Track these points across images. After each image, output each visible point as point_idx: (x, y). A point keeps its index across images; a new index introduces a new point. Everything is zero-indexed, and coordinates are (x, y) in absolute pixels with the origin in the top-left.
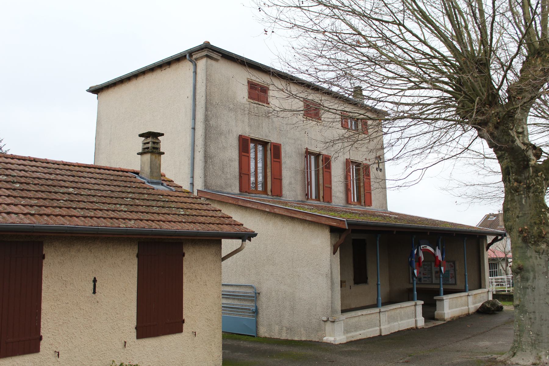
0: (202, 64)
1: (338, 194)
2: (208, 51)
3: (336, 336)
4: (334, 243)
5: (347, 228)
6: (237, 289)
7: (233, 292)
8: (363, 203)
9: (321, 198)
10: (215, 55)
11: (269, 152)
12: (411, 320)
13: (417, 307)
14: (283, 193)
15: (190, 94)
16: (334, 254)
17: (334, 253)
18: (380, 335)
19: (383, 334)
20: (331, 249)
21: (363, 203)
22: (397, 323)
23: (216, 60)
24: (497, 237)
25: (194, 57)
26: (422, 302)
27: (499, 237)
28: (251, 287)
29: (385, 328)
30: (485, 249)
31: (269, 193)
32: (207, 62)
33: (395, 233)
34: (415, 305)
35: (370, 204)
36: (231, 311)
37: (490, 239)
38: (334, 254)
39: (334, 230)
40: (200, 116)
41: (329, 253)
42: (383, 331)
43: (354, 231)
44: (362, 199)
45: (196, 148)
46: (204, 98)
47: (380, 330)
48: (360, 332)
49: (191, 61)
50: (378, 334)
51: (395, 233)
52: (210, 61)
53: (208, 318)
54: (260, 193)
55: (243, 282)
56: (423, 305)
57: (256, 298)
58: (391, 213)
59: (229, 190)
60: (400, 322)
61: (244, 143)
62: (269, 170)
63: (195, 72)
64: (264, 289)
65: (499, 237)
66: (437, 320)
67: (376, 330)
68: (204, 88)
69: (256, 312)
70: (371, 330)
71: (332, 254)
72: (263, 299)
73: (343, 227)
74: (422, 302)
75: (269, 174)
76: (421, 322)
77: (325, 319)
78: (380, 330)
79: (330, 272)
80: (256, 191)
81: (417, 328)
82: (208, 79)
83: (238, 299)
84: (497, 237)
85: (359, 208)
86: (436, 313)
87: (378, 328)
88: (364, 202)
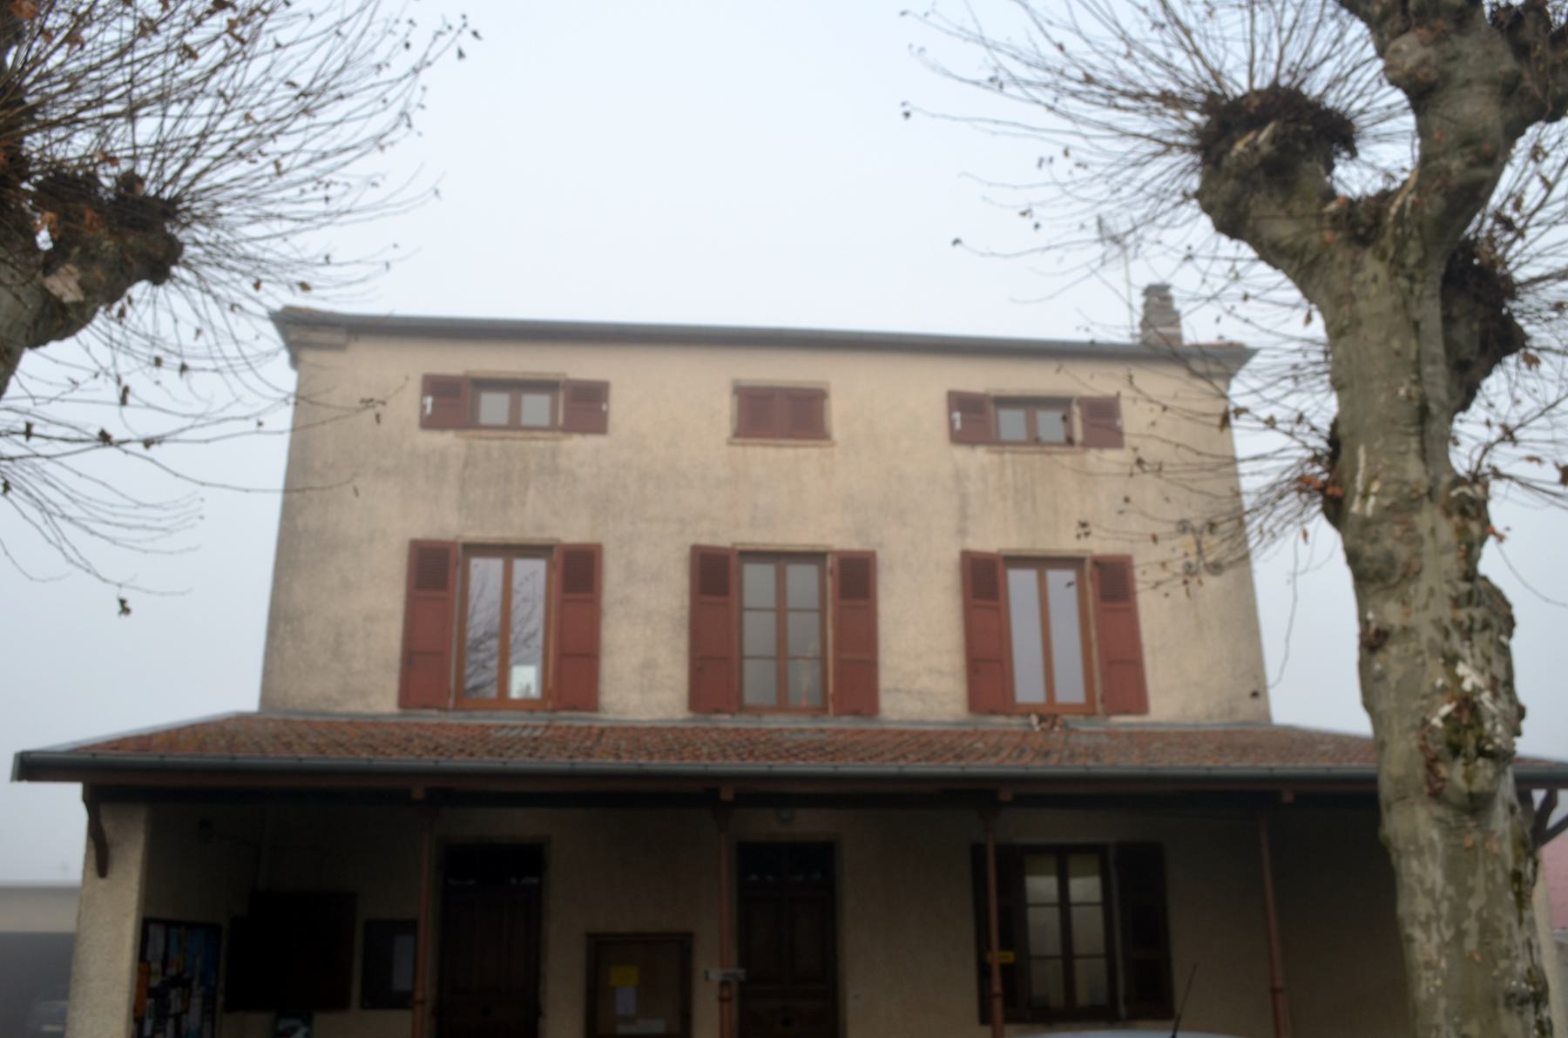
23: (340, 347)
35: (1139, 703)
59: (355, 706)
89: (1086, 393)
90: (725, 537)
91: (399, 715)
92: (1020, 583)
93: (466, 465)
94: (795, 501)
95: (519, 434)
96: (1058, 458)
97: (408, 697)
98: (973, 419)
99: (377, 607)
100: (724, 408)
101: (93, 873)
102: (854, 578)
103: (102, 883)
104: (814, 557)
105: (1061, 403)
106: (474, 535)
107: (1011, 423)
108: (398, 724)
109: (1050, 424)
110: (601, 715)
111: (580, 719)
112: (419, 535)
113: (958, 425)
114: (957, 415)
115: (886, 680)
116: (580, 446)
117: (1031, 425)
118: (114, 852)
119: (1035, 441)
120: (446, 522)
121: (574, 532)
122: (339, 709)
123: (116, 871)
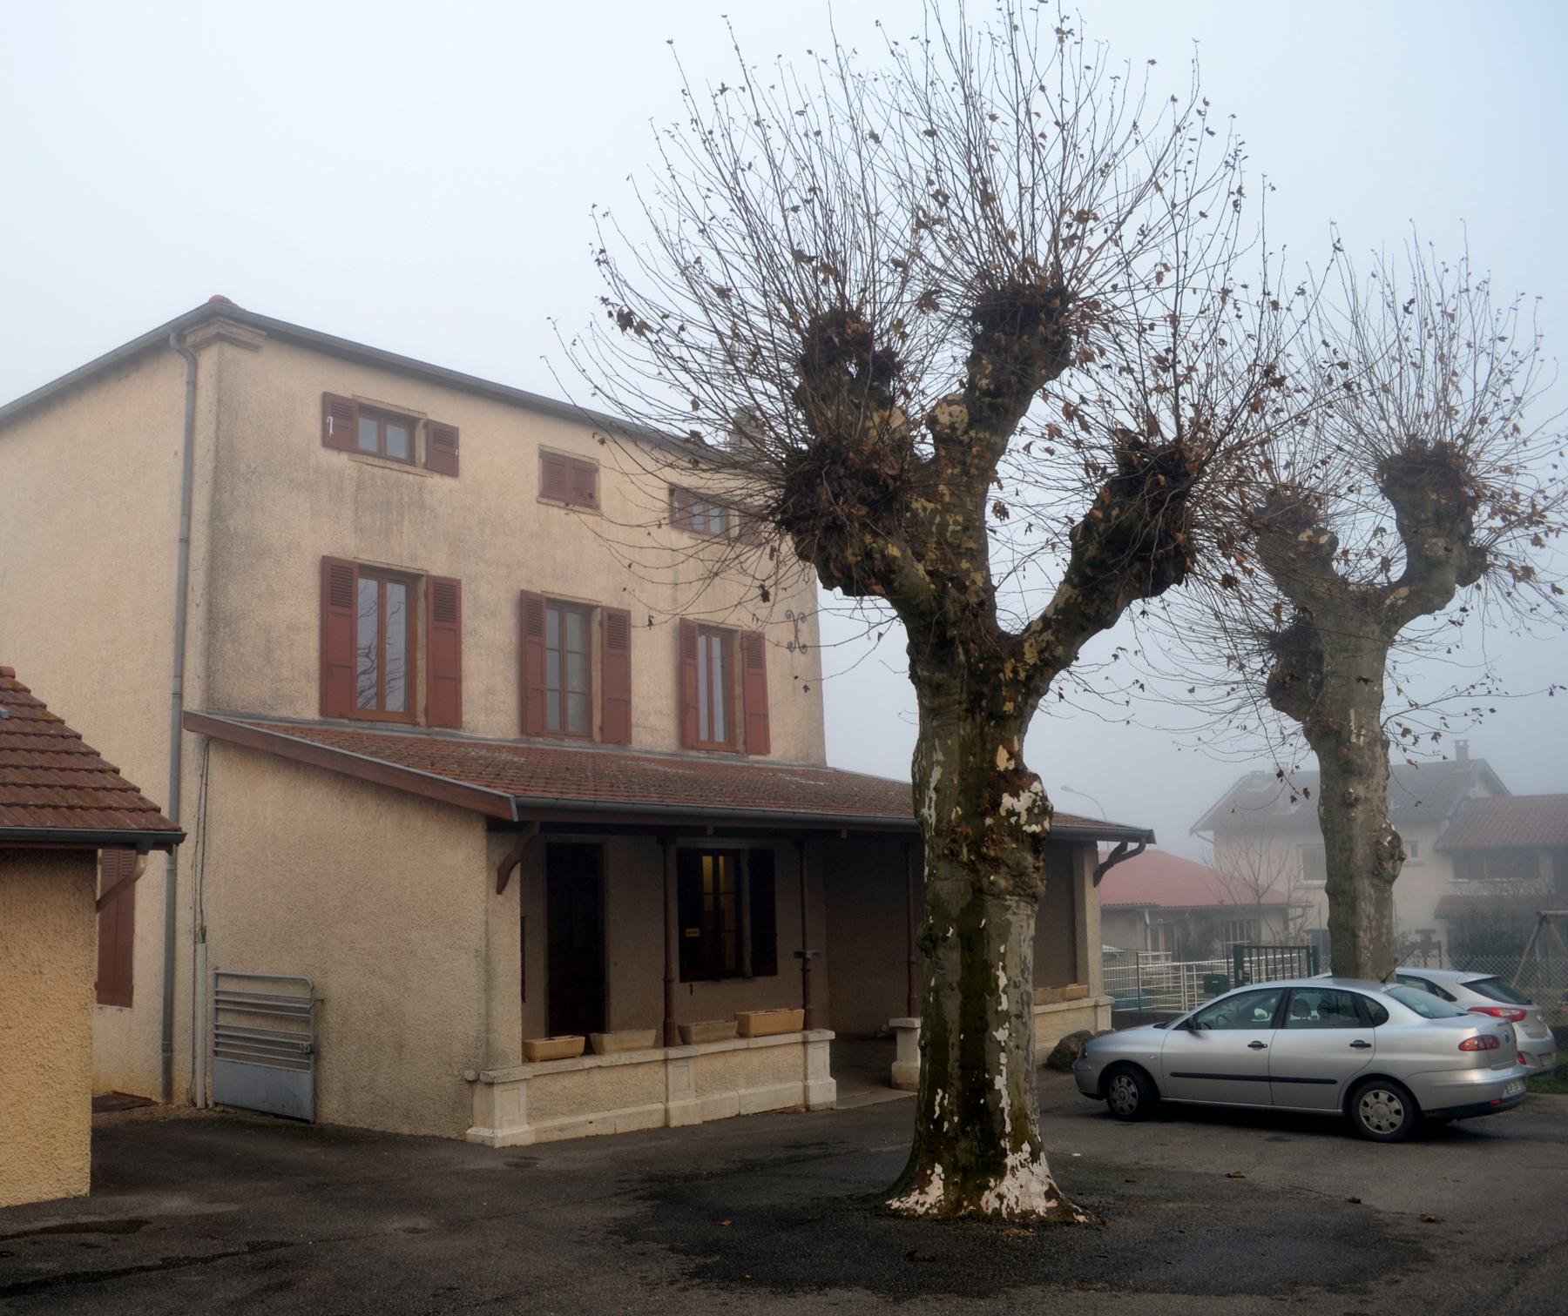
0: (208, 360)
1: (653, 720)
2: (218, 325)
3: (510, 1122)
4: (498, 859)
5: (516, 819)
6: (275, 990)
7: (266, 997)
8: (740, 747)
9: (596, 730)
10: (245, 334)
11: (422, 603)
12: (792, 1084)
13: (810, 1048)
14: (466, 718)
15: (179, 444)
16: (500, 890)
17: (500, 890)
18: (667, 1126)
19: (674, 1123)
20: (488, 877)
21: (740, 747)
22: (733, 1094)
23: (254, 348)
24: (1123, 847)
25: (190, 340)
26: (831, 1035)
27: (1132, 846)
28: (302, 982)
29: (685, 1108)
30: (1089, 880)
31: (422, 720)
32: (220, 354)
33: (844, 835)
34: (805, 1043)
35: (764, 749)
36: (259, 1050)
37: (1105, 848)
38: (500, 890)
39: (496, 826)
40: (201, 506)
41: (483, 888)
42: (672, 1114)
43: (546, 827)
44: (740, 732)
45: (191, 596)
46: (211, 456)
47: (667, 1111)
48: (592, 1117)
49: (182, 352)
50: (658, 1124)
51: (844, 835)
52: (231, 352)
53: (45, 1062)
54: (394, 718)
55: (287, 969)
56: (832, 1042)
57: (316, 1014)
58: (838, 774)
59: (285, 712)
60: (742, 1092)
61: (338, 581)
62: (421, 655)
63: (193, 384)
64: (336, 986)
65: (1132, 846)
66: (898, 1087)
67: (651, 1113)
68: (213, 428)
69: (313, 1052)
70: (632, 1110)
71: (493, 891)
72: (332, 1016)
73: (505, 816)
74: (831, 1035)
75: (421, 665)
76: (823, 1089)
77: (470, 1075)
78: (667, 1111)
79: (483, 943)
80: (380, 714)
81: (808, 1108)
82: (224, 404)
83: (276, 1017)
84: (1123, 847)
85: (726, 758)
86: (895, 1066)
87: (661, 1106)
88: (745, 743)
89: (433, 417)
91: (519, 741)
92: (366, 589)
93: (358, 489)
95: (381, 462)
96: (583, 517)
97: (324, 709)
98: (343, 422)
102: (617, 627)
103: (500, 897)
104: (409, 579)
105: (408, 422)
106: (367, 557)
107: (367, 430)
108: (515, 751)
109: (396, 438)
110: (461, 733)
111: (442, 734)
112: (326, 553)
114: (331, 419)
115: (636, 717)
116: (439, 484)
117: (382, 440)
119: (381, 454)
120: (350, 547)
121: (438, 567)
122: (273, 714)
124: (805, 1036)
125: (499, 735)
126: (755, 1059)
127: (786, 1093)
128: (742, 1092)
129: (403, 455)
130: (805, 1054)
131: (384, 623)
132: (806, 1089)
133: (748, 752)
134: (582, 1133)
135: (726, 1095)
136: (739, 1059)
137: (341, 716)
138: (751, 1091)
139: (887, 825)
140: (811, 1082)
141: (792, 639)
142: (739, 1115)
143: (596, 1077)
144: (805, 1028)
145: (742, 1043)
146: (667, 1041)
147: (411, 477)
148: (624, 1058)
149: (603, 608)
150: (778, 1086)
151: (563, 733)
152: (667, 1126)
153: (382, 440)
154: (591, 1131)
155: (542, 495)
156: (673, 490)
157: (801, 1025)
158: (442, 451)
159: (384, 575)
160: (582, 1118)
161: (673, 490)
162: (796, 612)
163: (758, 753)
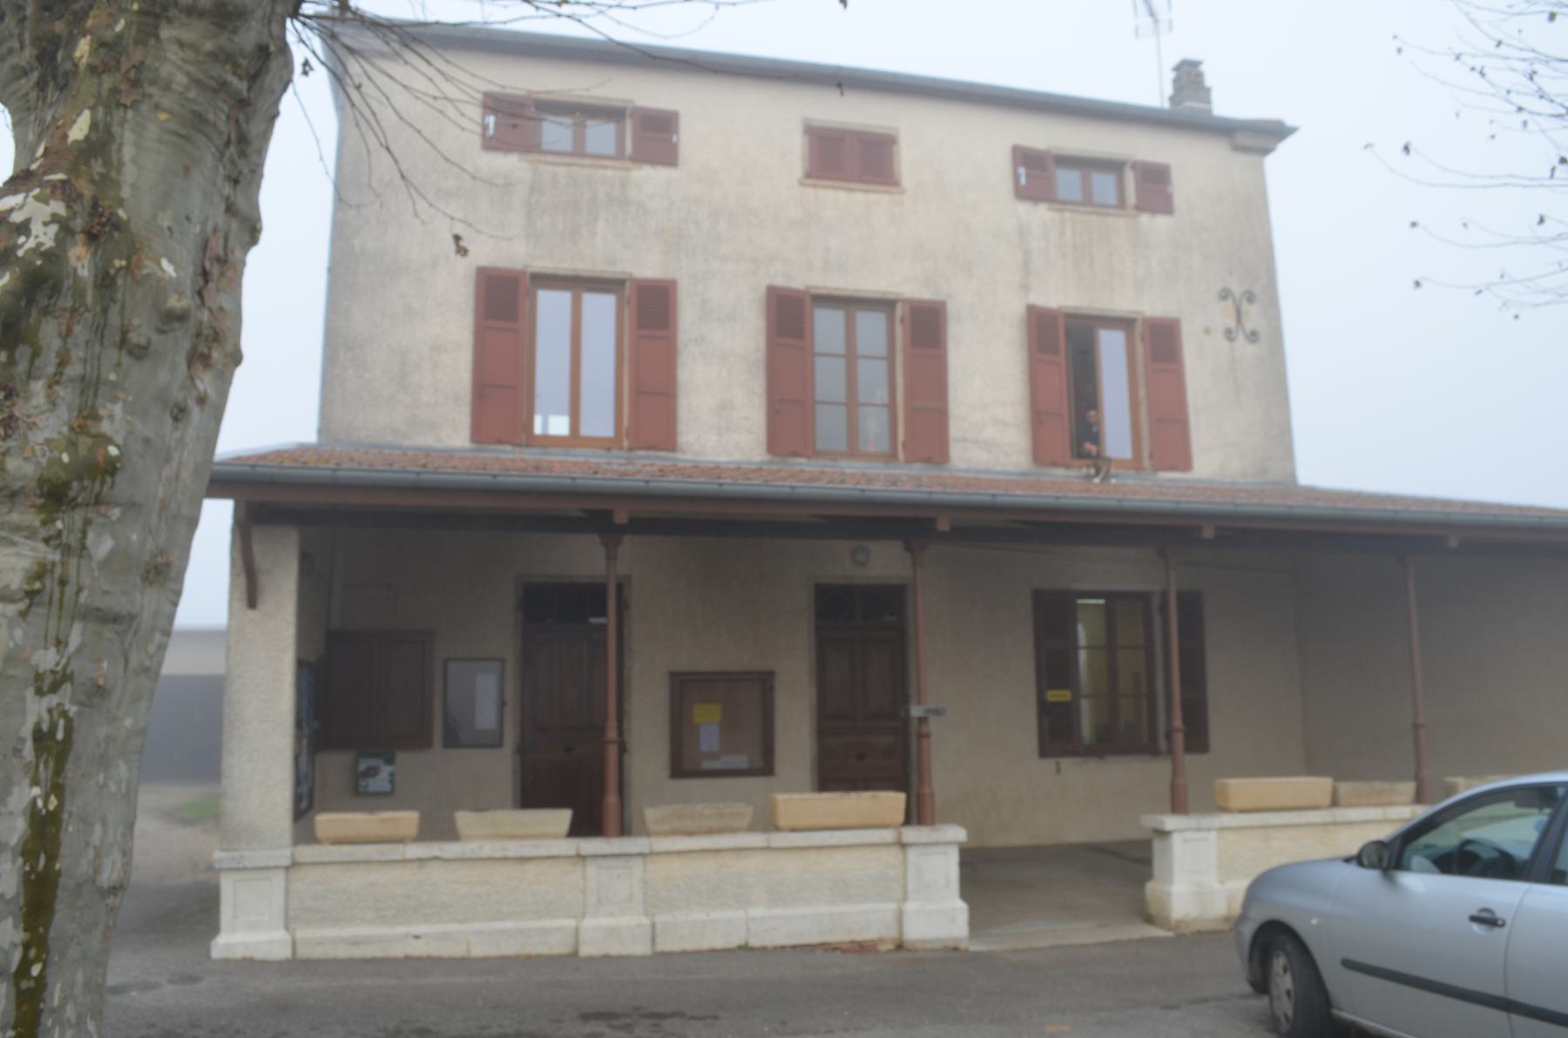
8: (1146, 463)
19: (585, 951)
35: (1185, 463)
58: (1311, 492)
59: (424, 440)
62: (1143, 412)
90: (799, 279)
92: (827, 327)
93: (532, 190)
94: (866, 246)
97: (479, 433)
99: (447, 332)
100: (795, 148)
101: (241, 605)
103: (252, 614)
104: (884, 304)
105: (1114, 166)
106: (543, 265)
107: (1068, 181)
110: (679, 455)
113: (1023, 181)
114: (1022, 171)
115: (955, 429)
116: (650, 178)
117: (1087, 189)
118: (263, 580)
120: (514, 251)
121: (648, 267)
122: (407, 443)
123: (267, 600)
124: (900, 835)
125: (737, 456)
126: (790, 866)
127: (865, 919)
128: (757, 912)
129: (1113, 200)
130: (905, 861)
131: (870, 362)
132: (900, 917)
133: (1157, 469)
134: (398, 951)
135: (717, 915)
136: (754, 862)
137: (500, 442)
138: (777, 911)
139: (513, 479)
140: (910, 906)
141: (1232, 323)
142: (744, 948)
143: (435, 872)
144: (908, 821)
145: (757, 839)
146: (580, 828)
147: (609, 173)
148: (488, 849)
149: (905, 301)
150: (843, 908)
151: (853, 452)
152: (575, 954)
153: (1087, 189)
154: (418, 949)
155: (809, 175)
156: (494, 103)
157: (901, 817)
158: (655, 137)
159: (850, 303)
160: (401, 930)
161: (494, 103)
162: (1237, 289)
163: (1173, 468)
